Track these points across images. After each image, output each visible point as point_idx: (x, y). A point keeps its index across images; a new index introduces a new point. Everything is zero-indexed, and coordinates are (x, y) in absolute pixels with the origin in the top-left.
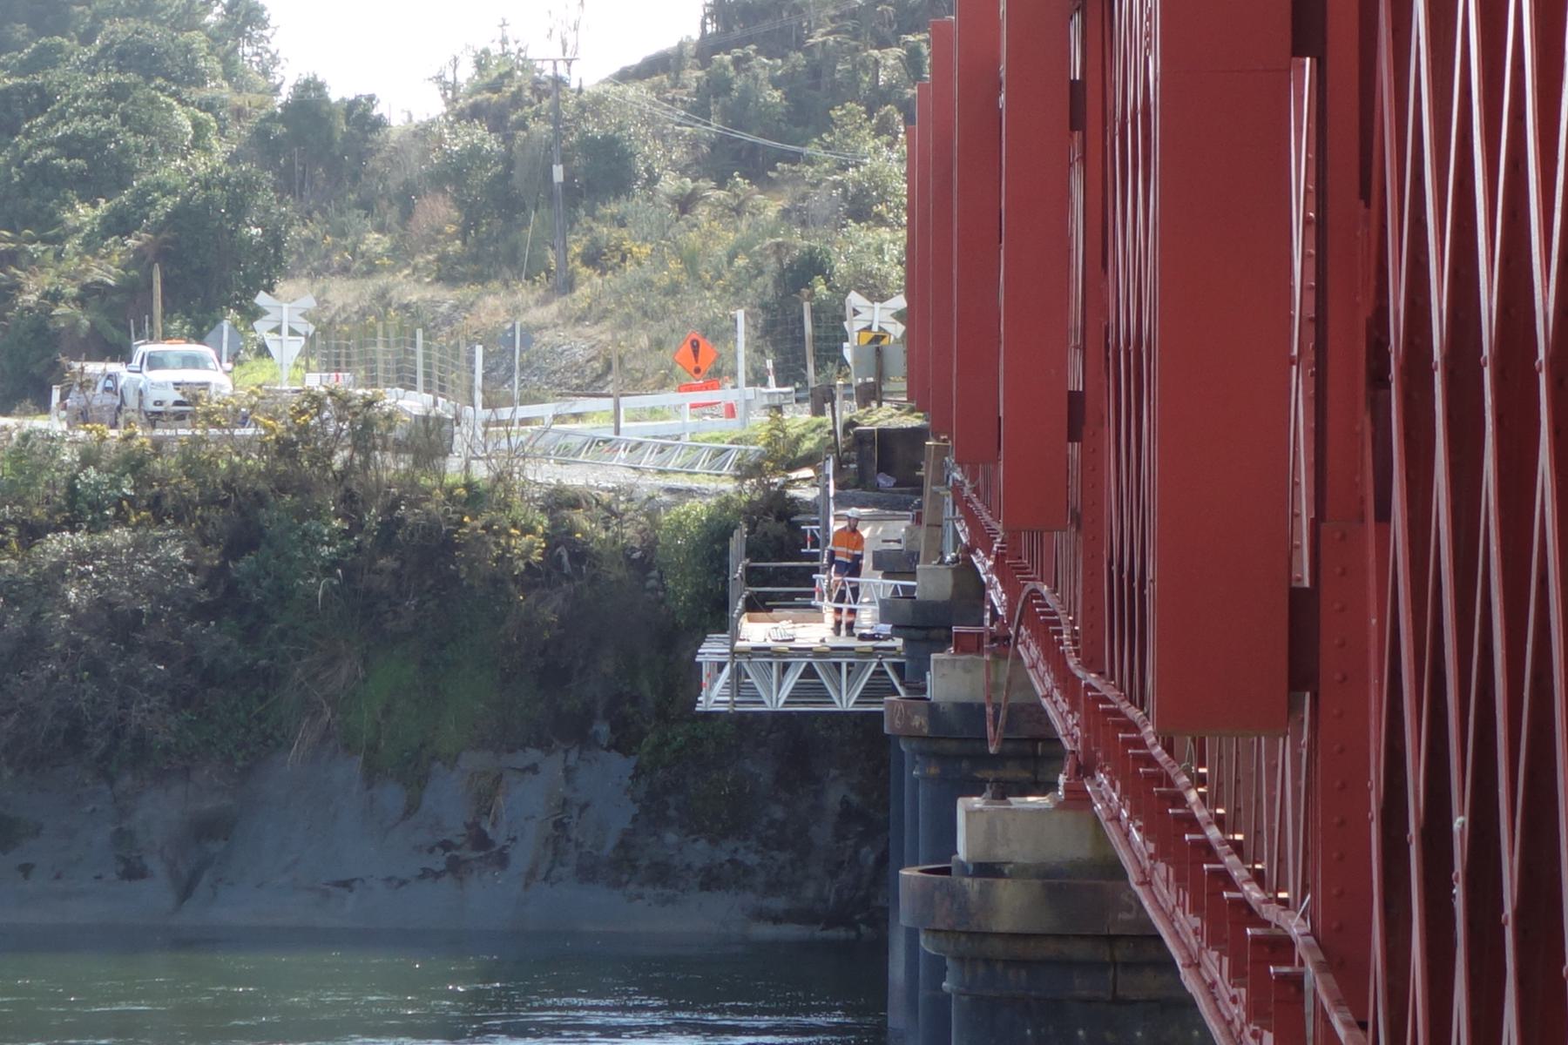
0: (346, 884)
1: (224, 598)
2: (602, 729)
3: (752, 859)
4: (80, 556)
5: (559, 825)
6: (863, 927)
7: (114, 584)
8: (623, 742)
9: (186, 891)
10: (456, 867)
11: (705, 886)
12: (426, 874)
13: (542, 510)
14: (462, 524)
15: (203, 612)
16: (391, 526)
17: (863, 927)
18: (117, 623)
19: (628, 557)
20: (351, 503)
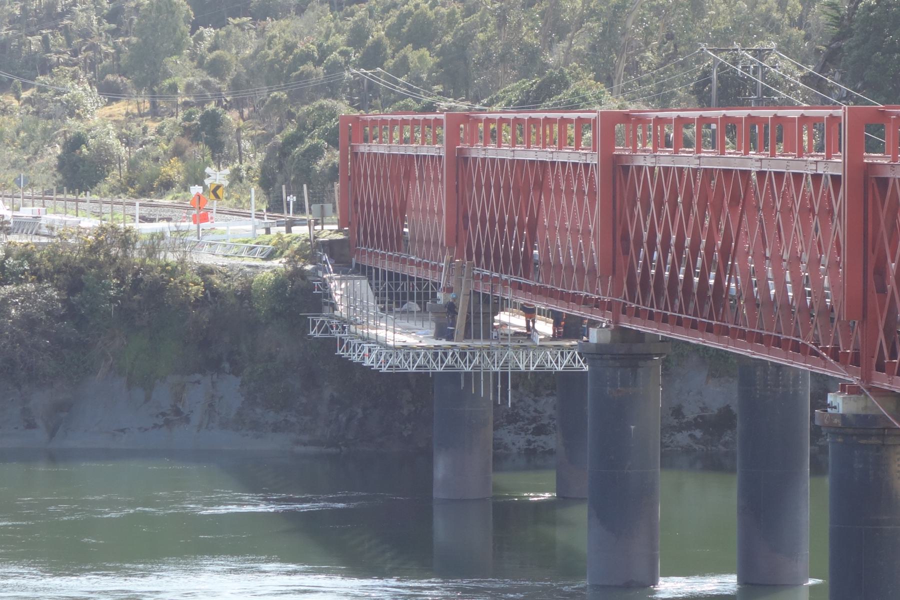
0: (123, 431)
1: (71, 312)
2: (226, 365)
3: (293, 419)
4: (13, 295)
5: (211, 405)
6: (343, 448)
7: (29, 308)
8: (236, 370)
9: (52, 434)
10: (168, 423)
11: (274, 431)
12: (155, 426)
13: (198, 274)
14: (171, 281)
15: (62, 318)
16: (137, 282)
17: (343, 448)
18: (29, 322)
19: (235, 295)
20: (120, 273)
